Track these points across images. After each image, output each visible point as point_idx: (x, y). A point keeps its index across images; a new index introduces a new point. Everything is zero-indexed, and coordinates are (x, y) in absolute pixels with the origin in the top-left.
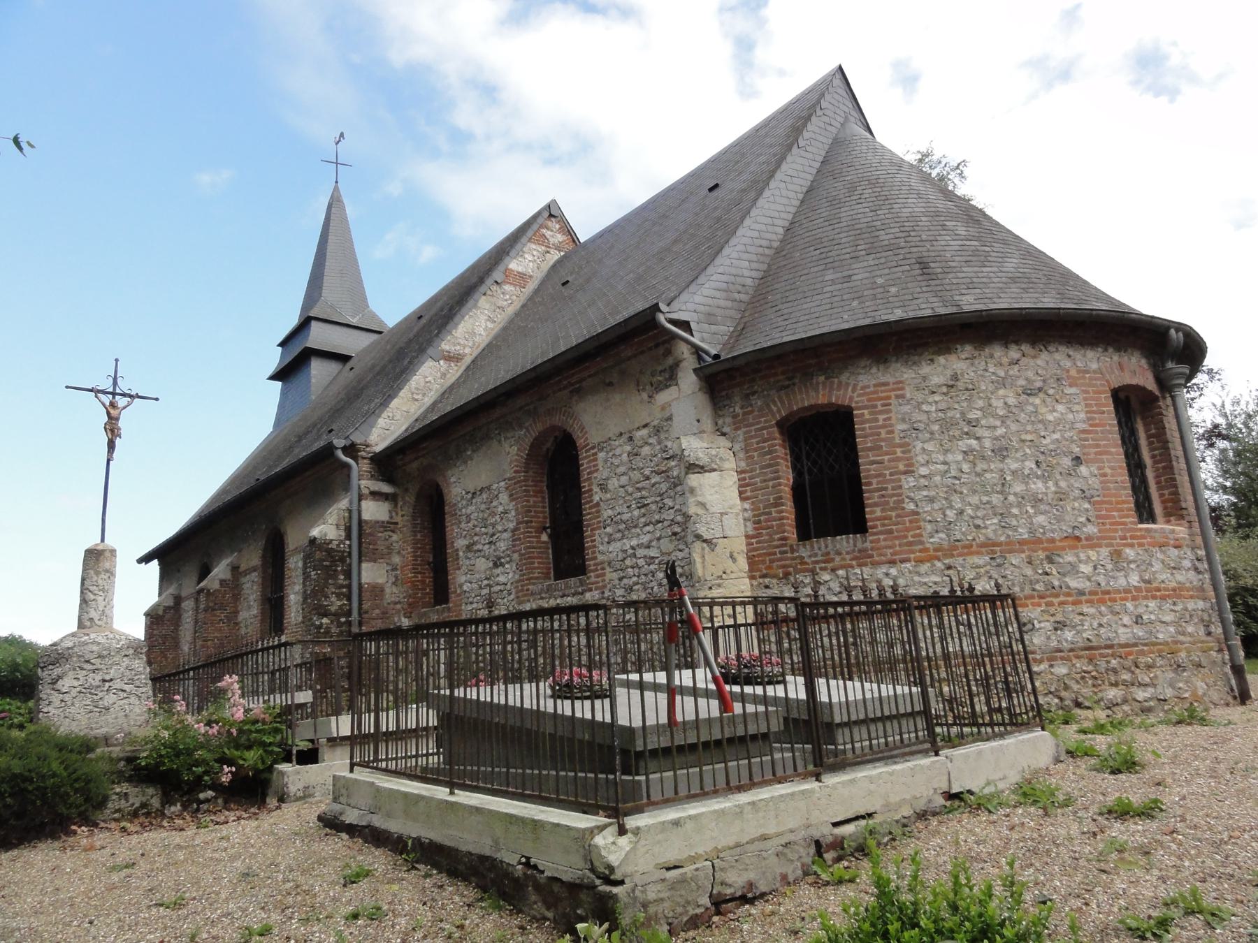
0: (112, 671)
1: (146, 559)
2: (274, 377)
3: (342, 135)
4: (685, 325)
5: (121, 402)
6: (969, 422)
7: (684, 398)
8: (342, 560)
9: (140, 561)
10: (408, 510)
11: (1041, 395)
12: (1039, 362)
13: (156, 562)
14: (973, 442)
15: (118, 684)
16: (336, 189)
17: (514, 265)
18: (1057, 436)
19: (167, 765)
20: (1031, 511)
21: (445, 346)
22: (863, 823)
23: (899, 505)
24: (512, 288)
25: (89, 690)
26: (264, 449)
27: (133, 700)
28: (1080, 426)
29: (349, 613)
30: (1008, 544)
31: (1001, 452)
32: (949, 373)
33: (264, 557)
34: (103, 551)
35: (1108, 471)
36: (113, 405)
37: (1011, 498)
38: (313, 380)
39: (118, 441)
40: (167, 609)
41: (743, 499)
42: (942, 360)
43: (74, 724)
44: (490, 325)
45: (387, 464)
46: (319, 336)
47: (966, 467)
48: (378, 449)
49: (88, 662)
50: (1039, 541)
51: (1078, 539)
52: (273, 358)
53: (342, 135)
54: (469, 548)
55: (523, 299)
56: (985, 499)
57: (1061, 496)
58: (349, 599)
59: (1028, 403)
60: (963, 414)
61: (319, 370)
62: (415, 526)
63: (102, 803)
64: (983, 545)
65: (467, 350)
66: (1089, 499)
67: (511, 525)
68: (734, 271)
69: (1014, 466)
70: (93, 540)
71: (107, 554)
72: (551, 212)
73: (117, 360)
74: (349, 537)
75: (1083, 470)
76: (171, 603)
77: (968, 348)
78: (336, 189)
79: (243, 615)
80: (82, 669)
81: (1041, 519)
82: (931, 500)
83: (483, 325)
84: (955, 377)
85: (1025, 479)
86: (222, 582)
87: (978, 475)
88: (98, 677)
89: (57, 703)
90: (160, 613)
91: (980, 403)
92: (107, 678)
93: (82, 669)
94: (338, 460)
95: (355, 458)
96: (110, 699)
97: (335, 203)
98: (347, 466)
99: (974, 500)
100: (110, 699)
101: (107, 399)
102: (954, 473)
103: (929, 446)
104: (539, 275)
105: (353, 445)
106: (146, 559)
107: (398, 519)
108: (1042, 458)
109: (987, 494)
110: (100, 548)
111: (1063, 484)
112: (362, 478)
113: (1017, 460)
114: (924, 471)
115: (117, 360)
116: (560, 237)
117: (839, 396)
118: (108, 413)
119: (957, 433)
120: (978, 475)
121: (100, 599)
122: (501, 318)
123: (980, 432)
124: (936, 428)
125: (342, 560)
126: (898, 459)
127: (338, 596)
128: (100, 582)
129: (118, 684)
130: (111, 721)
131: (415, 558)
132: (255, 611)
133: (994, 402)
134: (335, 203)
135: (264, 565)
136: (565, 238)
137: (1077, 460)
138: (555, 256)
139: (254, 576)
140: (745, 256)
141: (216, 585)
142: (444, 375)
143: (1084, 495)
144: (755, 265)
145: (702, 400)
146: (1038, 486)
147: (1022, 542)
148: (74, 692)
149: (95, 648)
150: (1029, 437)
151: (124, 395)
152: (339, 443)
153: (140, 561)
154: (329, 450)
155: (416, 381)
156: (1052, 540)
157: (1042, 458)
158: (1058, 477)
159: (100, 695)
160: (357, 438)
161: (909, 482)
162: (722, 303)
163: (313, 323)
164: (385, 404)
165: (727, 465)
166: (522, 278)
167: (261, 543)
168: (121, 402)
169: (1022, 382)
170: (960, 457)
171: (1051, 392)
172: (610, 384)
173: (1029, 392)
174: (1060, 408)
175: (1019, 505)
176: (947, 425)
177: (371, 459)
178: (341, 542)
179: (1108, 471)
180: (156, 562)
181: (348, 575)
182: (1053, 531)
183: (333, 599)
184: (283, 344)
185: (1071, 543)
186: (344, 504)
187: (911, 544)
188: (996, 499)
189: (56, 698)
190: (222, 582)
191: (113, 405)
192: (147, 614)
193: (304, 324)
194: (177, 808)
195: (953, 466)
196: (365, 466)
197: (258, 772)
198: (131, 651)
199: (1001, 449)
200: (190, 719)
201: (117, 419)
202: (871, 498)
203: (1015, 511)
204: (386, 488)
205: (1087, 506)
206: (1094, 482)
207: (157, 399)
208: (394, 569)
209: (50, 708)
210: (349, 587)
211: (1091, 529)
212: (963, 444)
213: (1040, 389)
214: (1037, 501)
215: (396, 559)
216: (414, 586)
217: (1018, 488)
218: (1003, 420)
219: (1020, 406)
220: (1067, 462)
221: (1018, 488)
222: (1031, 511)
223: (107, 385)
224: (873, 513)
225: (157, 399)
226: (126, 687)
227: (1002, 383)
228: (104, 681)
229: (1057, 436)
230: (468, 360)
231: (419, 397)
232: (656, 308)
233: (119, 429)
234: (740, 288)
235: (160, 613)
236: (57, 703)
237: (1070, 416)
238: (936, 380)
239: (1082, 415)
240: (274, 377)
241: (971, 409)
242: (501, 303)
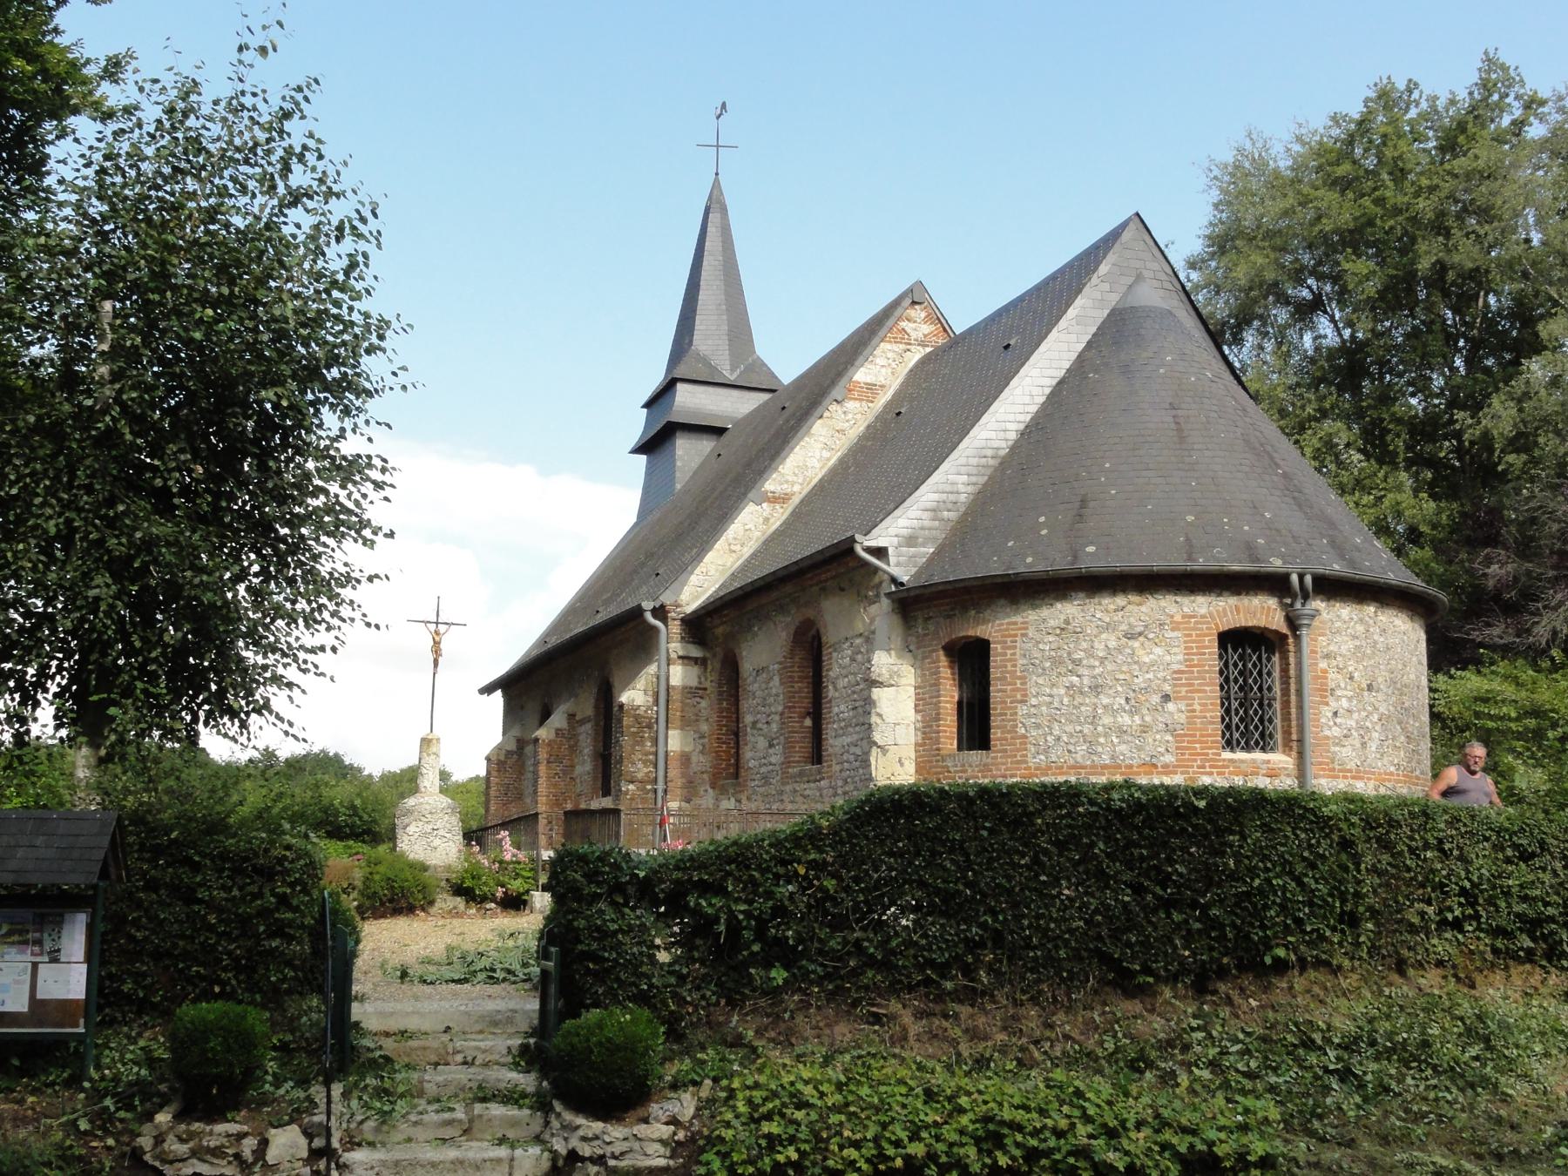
1: (488, 690)
2: (639, 450)
3: (724, 106)
4: (880, 552)
5: (442, 628)
6: (1073, 662)
7: (878, 615)
8: (649, 726)
10: (714, 676)
11: (1141, 639)
12: (1143, 609)
13: (499, 693)
14: (1075, 679)
15: (441, 832)
16: (716, 185)
17: (862, 375)
18: (1150, 676)
19: (467, 884)
20: (1116, 740)
21: (771, 485)
23: (1014, 729)
24: (857, 404)
26: (623, 550)
28: (1176, 667)
29: (655, 781)
30: (1092, 767)
31: (1096, 689)
32: (1063, 617)
33: (596, 707)
35: (1197, 707)
37: (1100, 729)
38: (679, 464)
40: (509, 753)
41: (917, 711)
42: (1059, 605)
44: (826, 454)
45: (698, 626)
46: (691, 401)
47: (1066, 700)
48: (689, 609)
50: (1120, 767)
51: (1155, 766)
52: (636, 425)
53: (724, 106)
54: (754, 723)
55: (870, 418)
56: (1078, 728)
57: (1145, 728)
58: (656, 767)
59: (1127, 646)
60: (1069, 654)
61: (688, 453)
62: (720, 693)
63: (431, 903)
64: (1073, 767)
65: (797, 488)
66: (1173, 732)
67: (780, 708)
68: (948, 488)
69: (1105, 701)
72: (915, 296)
74: (656, 702)
75: (1171, 706)
76: (512, 746)
77: (1081, 595)
78: (716, 185)
79: (579, 770)
81: (1123, 748)
82: (1038, 726)
83: (818, 455)
84: (1067, 622)
85: (1114, 713)
87: (1075, 707)
91: (1084, 645)
94: (645, 622)
95: (664, 619)
96: (437, 842)
97: (715, 206)
98: (655, 629)
99: (1069, 728)
100: (437, 842)
101: (432, 627)
102: (1056, 705)
103: (1040, 681)
104: (895, 384)
105: (662, 606)
106: (488, 690)
107: (707, 684)
108: (1132, 695)
109: (1080, 724)
111: (1147, 719)
112: (671, 641)
113: (1109, 696)
114: (1034, 701)
116: (926, 329)
117: (980, 631)
119: (1063, 670)
120: (1075, 707)
122: (842, 445)
123: (1081, 671)
124: (1048, 664)
125: (649, 726)
126: (1018, 690)
127: (645, 762)
129: (441, 832)
131: (720, 727)
132: (588, 767)
133: (1096, 645)
134: (715, 206)
135: (597, 714)
136: (932, 328)
137: (1166, 698)
138: (917, 355)
139: (588, 727)
140: (963, 470)
142: (767, 520)
143: (1167, 728)
144: (974, 479)
145: (896, 620)
146: (1125, 720)
147: (1104, 767)
150: (1122, 677)
152: (648, 605)
154: (637, 612)
155: (735, 530)
156: (1131, 766)
157: (1132, 695)
158: (1145, 711)
160: (666, 598)
161: (1022, 710)
162: (927, 523)
163: (680, 386)
164: (699, 557)
165: (903, 681)
166: (872, 389)
167: (595, 690)
168: (442, 628)
169: (1124, 627)
170: (1062, 691)
171: (1151, 636)
172: (842, 590)
173: (1130, 636)
174: (1158, 651)
175: (1106, 735)
176: (1058, 662)
177: (682, 620)
178: (649, 708)
179: (1197, 707)
180: (499, 693)
181: (655, 742)
182: (1132, 758)
183: (640, 765)
184: (649, 405)
185: (1147, 769)
186: (652, 669)
187: (1018, 762)
188: (1087, 729)
189: (406, 838)
190: (558, 732)
191: (437, 633)
192: (488, 759)
193: (669, 387)
194: (473, 911)
195: (1056, 701)
196: (676, 628)
197: (520, 895)
199: (1097, 687)
200: (480, 857)
202: (995, 721)
203: (1102, 740)
204: (696, 652)
205: (1169, 737)
206: (1182, 718)
208: (702, 737)
210: (656, 754)
211: (1169, 759)
212: (1066, 681)
213: (1140, 634)
214: (1121, 731)
215: (704, 727)
216: (718, 757)
217: (1107, 720)
218: (1102, 660)
219: (1119, 650)
220: (1156, 699)
221: (1107, 720)
222: (1116, 740)
224: (995, 734)
227: (1108, 627)
229: (1150, 676)
230: (796, 500)
231: (738, 548)
232: (852, 540)
234: (950, 506)
237: (1168, 658)
238: (1052, 623)
239: (1180, 657)
240: (639, 450)
241: (1077, 649)
242: (840, 426)
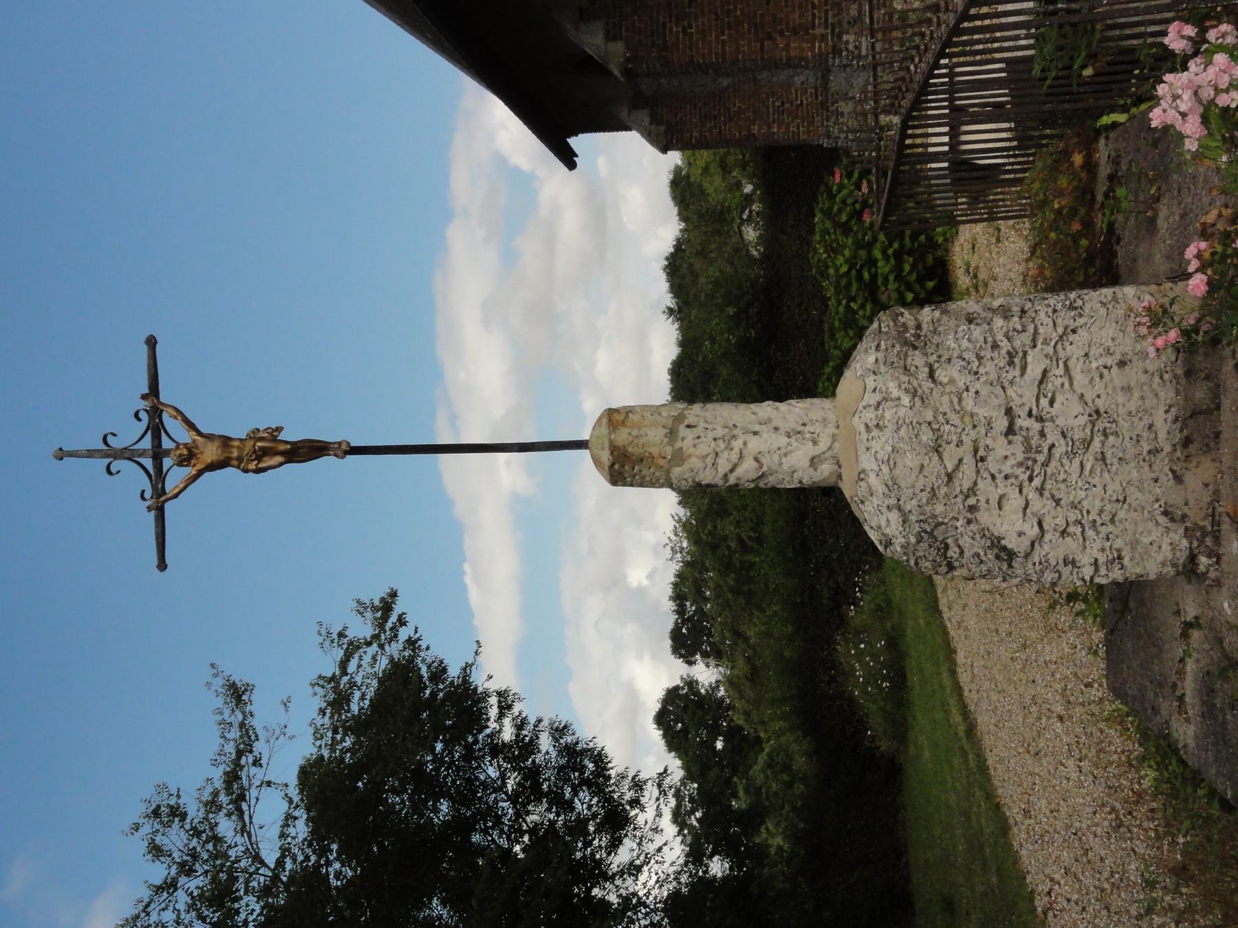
0: (982, 412)
9: (571, 165)
13: (573, 142)
15: (1023, 393)
22: (261, 465)
25: (1034, 462)
27: (1073, 350)
34: (614, 449)
36: (188, 457)
39: (291, 434)
40: (654, 120)
43: (1134, 496)
49: (950, 477)
70: (584, 470)
71: (622, 437)
73: (61, 455)
80: (972, 491)
86: (610, 37)
88: (1000, 447)
89: (1070, 546)
90: (662, 128)
92: (1003, 423)
93: (972, 491)
96: (1069, 413)
110: (606, 457)
115: (61, 455)
118: (212, 467)
121: (754, 444)
128: (705, 448)
129: (1023, 393)
130: (1133, 405)
141: (618, 47)
148: (1037, 504)
149: (910, 460)
151: (156, 429)
153: (571, 165)
159: (1053, 436)
180: (573, 142)
190: (610, 37)
198: (917, 359)
201: (226, 441)
207: (152, 342)
209: (1085, 560)
223: (133, 478)
225: (152, 342)
226: (1034, 371)
228: (1010, 431)
233: (254, 435)
235: (662, 128)
236: (1070, 546)
